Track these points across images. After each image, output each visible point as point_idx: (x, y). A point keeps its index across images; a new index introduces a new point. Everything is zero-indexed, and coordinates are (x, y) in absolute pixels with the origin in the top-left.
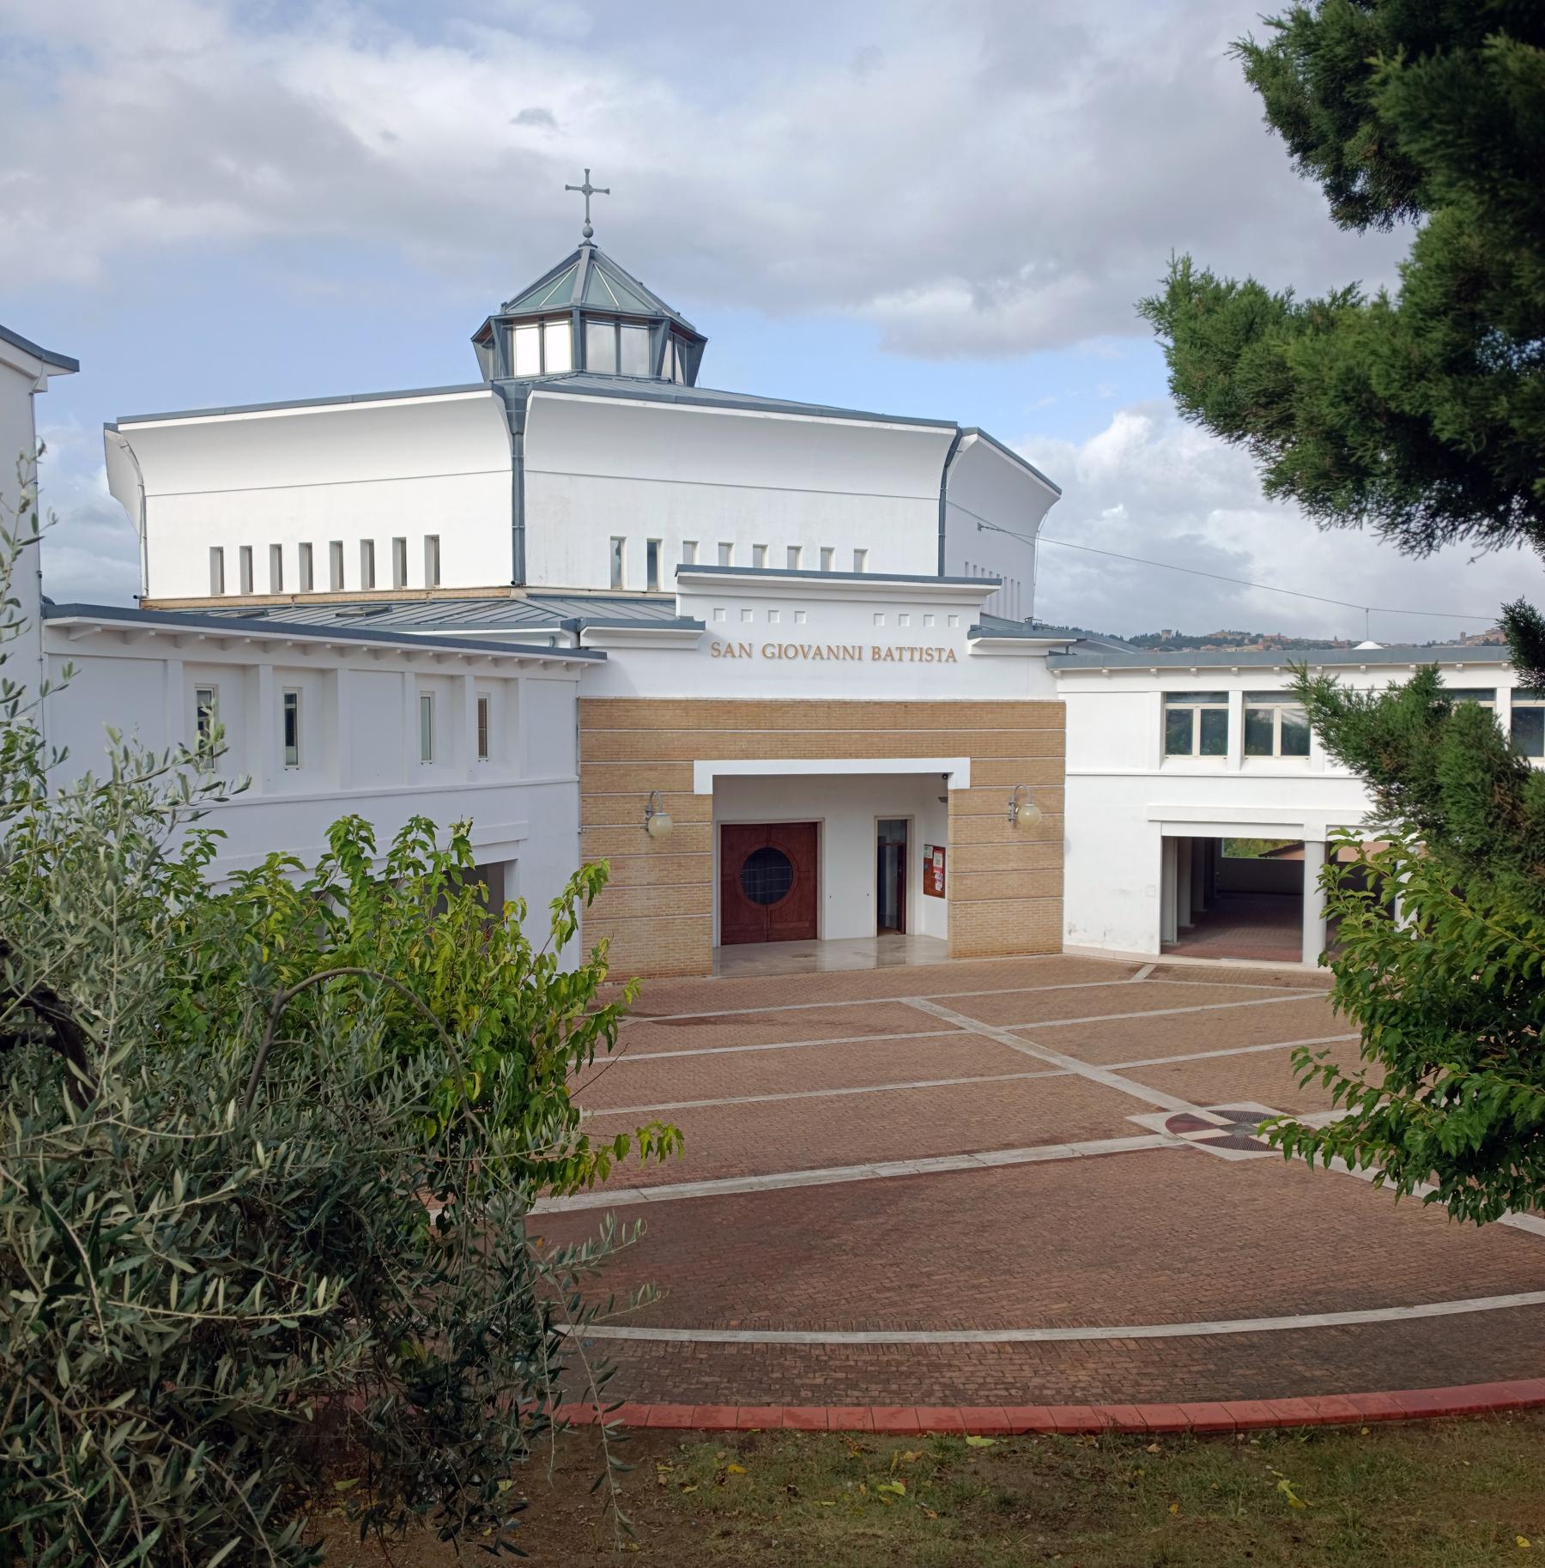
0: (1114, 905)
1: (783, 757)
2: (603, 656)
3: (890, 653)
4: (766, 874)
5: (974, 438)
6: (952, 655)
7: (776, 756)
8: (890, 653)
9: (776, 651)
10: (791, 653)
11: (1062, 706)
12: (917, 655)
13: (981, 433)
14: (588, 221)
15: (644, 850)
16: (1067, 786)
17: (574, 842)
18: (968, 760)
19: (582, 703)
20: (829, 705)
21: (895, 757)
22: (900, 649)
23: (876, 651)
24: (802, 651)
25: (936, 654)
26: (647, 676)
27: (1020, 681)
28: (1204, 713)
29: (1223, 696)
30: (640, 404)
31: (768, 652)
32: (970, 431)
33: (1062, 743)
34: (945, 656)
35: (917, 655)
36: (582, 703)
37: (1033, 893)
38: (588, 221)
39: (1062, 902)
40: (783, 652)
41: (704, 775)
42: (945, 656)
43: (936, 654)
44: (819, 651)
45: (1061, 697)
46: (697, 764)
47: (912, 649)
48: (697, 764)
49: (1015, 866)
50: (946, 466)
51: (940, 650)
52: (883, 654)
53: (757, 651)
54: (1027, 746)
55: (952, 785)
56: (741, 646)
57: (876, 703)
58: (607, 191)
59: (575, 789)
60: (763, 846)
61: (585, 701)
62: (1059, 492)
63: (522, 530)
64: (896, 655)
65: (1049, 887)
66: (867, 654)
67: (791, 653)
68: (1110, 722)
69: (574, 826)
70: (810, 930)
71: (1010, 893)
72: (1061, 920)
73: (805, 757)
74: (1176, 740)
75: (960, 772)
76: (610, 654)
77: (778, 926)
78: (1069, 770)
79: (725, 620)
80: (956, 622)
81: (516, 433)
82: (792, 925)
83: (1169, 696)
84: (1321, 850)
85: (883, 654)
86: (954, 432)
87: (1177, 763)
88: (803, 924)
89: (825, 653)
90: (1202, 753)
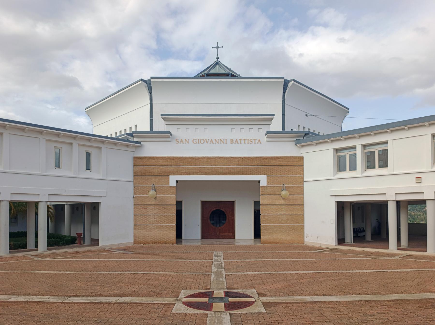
0: (320, 227)
1: (199, 175)
2: (140, 143)
3: (237, 141)
4: (218, 219)
5: (292, 82)
6: (259, 141)
7: (197, 174)
8: (237, 141)
9: (197, 141)
10: (202, 141)
11: (303, 157)
12: (246, 142)
13: (294, 80)
14: (217, 55)
15: (153, 203)
16: (304, 186)
17: (132, 200)
18: (266, 176)
19: (135, 158)
20: (215, 158)
21: (239, 175)
22: (241, 140)
23: (232, 141)
24: (206, 141)
25: (253, 141)
26: (152, 150)
27: (286, 149)
28: (350, 155)
29: (354, 148)
30: (182, 80)
31: (195, 141)
32: (291, 81)
33: (303, 171)
34: (257, 141)
35: (246, 142)
36: (135, 158)
37: (292, 222)
38: (217, 55)
39: (304, 226)
40: (199, 141)
41: (173, 180)
42: (257, 141)
43: (253, 141)
44: (212, 141)
45: (302, 155)
46: (170, 176)
47: (245, 140)
48: (170, 176)
49: (285, 213)
50: (284, 93)
51: (255, 140)
52: (234, 141)
53: (191, 141)
54: (290, 172)
55: (261, 184)
56: (185, 140)
57: (232, 157)
58: (223, 47)
59: (132, 184)
60: (217, 209)
61: (137, 157)
62: (348, 109)
63: (152, 119)
64: (239, 141)
65: (299, 221)
66: (229, 142)
67: (202, 141)
68: (318, 162)
69: (132, 196)
70: (232, 236)
71: (283, 222)
72: (304, 233)
73: (207, 175)
74: (340, 166)
75: (263, 180)
76: (142, 143)
77: (222, 234)
78: (305, 180)
79: (178, 131)
80: (261, 131)
81: (151, 93)
82: (226, 234)
83: (337, 150)
84: (395, 203)
85: (234, 141)
86: (283, 80)
87: (342, 175)
88: (230, 233)
89: (214, 141)
90: (350, 170)
